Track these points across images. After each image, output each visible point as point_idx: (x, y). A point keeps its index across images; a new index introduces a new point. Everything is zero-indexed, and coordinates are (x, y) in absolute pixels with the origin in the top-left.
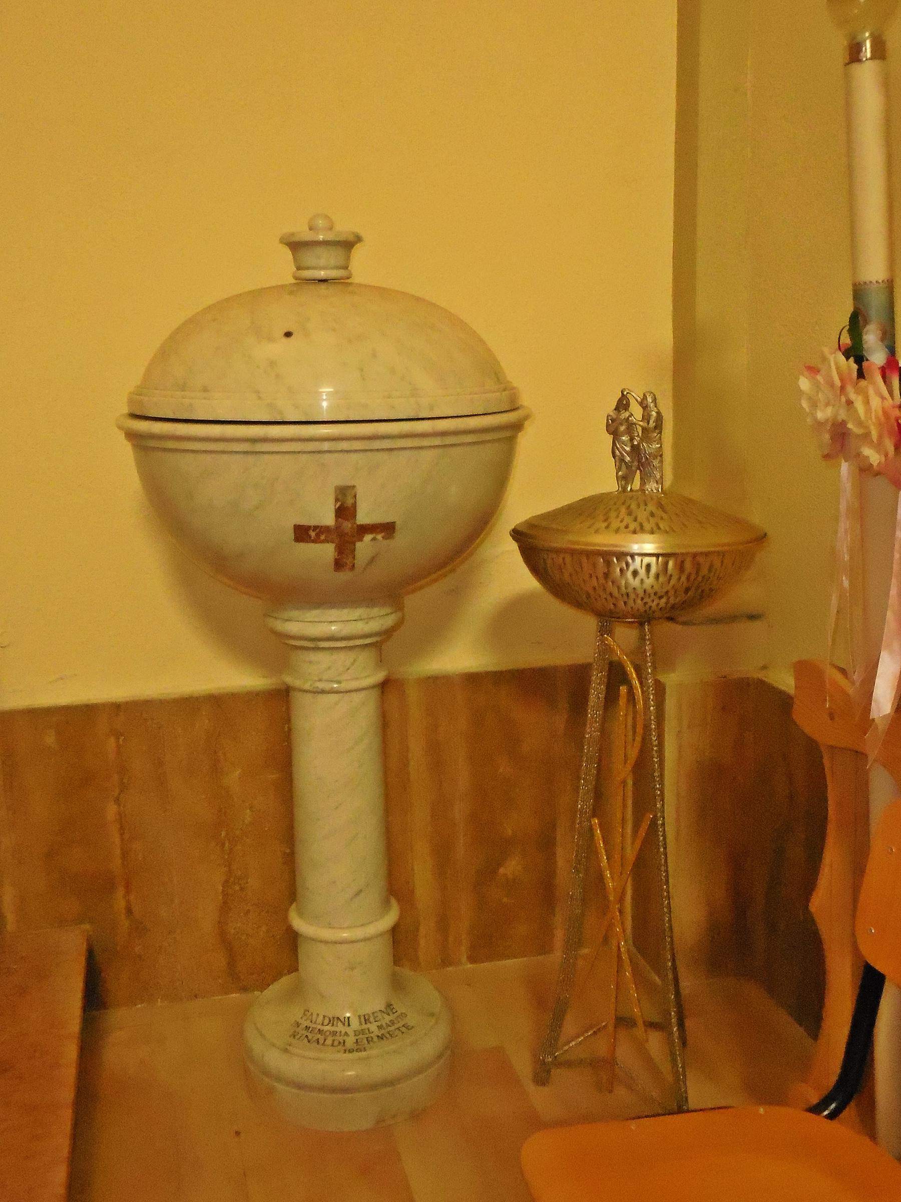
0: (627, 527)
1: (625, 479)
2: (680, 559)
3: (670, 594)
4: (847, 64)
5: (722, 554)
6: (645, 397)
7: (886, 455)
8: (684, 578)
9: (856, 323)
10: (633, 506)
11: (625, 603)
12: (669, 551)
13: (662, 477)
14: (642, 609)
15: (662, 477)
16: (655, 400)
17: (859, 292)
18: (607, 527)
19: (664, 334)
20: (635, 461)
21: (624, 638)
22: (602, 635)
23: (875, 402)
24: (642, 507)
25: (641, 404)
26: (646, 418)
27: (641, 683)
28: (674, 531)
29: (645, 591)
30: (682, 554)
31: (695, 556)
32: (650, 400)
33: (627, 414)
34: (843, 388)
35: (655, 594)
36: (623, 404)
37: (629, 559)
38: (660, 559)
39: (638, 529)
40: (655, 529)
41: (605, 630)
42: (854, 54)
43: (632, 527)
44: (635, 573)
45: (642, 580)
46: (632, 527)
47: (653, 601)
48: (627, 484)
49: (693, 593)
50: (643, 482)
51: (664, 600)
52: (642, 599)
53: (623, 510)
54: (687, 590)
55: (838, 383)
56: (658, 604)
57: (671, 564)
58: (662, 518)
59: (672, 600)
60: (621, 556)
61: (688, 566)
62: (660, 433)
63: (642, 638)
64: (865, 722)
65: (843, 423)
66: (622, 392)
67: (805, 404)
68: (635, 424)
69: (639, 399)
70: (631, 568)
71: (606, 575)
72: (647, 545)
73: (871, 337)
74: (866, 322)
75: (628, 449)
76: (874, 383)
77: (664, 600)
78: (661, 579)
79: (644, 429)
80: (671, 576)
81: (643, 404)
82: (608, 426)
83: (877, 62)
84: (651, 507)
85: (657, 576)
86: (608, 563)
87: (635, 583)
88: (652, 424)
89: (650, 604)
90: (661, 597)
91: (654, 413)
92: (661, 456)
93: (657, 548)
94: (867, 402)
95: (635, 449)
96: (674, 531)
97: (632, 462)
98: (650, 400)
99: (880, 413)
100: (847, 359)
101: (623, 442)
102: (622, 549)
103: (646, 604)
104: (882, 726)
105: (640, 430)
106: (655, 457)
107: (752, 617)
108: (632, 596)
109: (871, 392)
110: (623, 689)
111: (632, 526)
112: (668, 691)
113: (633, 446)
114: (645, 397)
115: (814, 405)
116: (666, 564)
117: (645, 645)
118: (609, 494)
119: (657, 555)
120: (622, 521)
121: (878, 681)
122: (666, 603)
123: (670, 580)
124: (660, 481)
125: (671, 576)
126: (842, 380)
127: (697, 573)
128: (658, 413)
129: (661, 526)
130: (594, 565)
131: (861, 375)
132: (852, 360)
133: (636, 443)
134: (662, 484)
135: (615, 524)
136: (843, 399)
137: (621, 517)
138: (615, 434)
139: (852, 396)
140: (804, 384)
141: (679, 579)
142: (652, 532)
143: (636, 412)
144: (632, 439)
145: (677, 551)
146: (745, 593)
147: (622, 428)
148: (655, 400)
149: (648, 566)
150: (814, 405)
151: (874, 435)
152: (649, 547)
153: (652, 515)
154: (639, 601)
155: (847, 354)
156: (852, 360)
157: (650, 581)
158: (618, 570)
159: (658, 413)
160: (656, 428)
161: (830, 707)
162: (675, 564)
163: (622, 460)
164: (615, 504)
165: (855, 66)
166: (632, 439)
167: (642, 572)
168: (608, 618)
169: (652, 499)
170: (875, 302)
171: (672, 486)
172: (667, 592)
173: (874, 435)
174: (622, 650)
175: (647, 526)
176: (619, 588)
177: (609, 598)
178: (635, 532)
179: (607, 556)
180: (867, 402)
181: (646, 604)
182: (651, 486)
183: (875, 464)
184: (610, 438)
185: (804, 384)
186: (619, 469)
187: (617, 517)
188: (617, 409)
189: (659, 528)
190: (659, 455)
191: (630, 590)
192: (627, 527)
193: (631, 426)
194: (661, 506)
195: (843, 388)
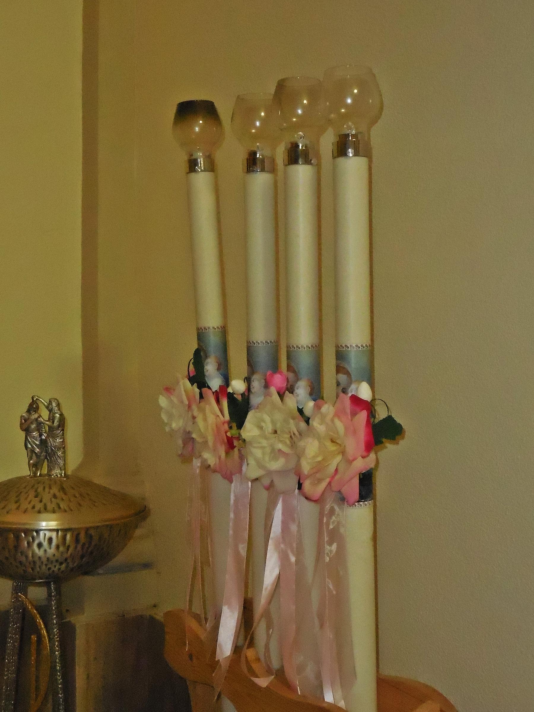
0: (33, 507)
1: (36, 466)
2: (75, 533)
3: (69, 561)
4: (188, 173)
5: (111, 526)
6: (50, 403)
7: (220, 458)
8: (79, 547)
9: (199, 358)
10: (40, 489)
11: (33, 569)
12: (66, 526)
13: (64, 465)
14: (47, 572)
15: (64, 465)
16: (58, 405)
17: (201, 335)
18: (18, 508)
19: (75, 345)
20: (44, 454)
21: (37, 593)
22: (17, 593)
23: (211, 419)
24: (47, 490)
25: (47, 407)
26: (52, 419)
27: (48, 632)
28: (71, 510)
29: (48, 559)
30: (78, 529)
31: (87, 529)
32: (54, 404)
33: (36, 416)
34: (189, 406)
35: (57, 561)
36: (33, 407)
37: (35, 534)
38: (60, 533)
39: (42, 509)
40: (56, 509)
41: (20, 589)
42: (192, 165)
43: (37, 508)
44: (40, 545)
45: (45, 551)
46: (37, 508)
47: (55, 566)
48: (37, 469)
49: (92, 553)
50: (50, 470)
51: (64, 566)
52: (46, 565)
53: (32, 494)
54: (82, 557)
55: (187, 402)
56: (59, 569)
57: (68, 537)
58: (63, 499)
59: (71, 565)
60: (28, 532)
61: (82, 536)
62: (63, 430)
63: (50, 595)
64: (214, 664)
65: (189, 433)
66: (33, 398)
67: (164, 417)
68: (42, 423)
69: (46, 404)
70: (36, 542)
71: (16, 547)
72: (48, 524)
73: (210, 367)
74: (207, 357)
75: (38, 443)
76: (210, 404)
77: (63, 566)
78: (61, 549)
79: (50, 427)
80: (69, 546)
81: (49, 408)
82: (21, 424)
83: (207, 173)
84: (55, 490)
85: (58, 547)
86: (18, 538)
87: (40, 553)
88: (56, 423)
89: (53, 568)
90: (61, 564)
91: (58, 415)
92: (64, 448)
93: (57, 525)
94: (205, 419)
95: (44, 443)
96: (71, 510)
97: (41, 453)
98: (54, 404)
99: (214, 426)
100: (192, 385)
101: (34, 437)
102: (27, 527)
103: (49, 569)
104: (224, 666)
105: (47, 428)
106: (59, 449)
107: (147, 566)
108: (38, 564)
109: (207, 411)
110: (34, 638)
111: (39, 506)
112: (78, 631)
113: (41, 440)
114: (50, 403)
115: (171, 416)
116: (64, 538)
117: (51, 600)
118: (20, 479)
119: (57, 531)
120: (30, 503)
121: (221, 630)
122: (67, 567)
123: (68, 549)
124: (64, 468)
125: (69, 546)
126: (188, 399)
127: (90, 543)
128: (61, 415)
129: (61, 506)
130: (7, 539)
131: (201, 396)
132: (195, 384)
133: (43, 437)
134: (65, 469)
135: (25, 505)
136: (190, 414)
137: (29, 499)
138: (27, 431)
139: (196, 413)
140: (163, 401)
141: (76, 547)
142: (54, 512)
143: (45, 414)
144: (41, 435)
145: (73, 526)
146: (137, 548)
147: (33, 426)
148: (58, 405)
149: (50, 540)
150: (171, 416)
151: (210, 443)
152: (53, 524)
153: (55, 496)
154: (44, 567)
155: (192, 380)
156: (195, 384)
157: (52, 551)
158: (26, 543)
159: (61, 415)
160: (59, 426)
161: (189, 650)
162: (72, 536)
163: (33, 451)
164: (25, 488)
165: (193, 175)
166: (41, 435)
167: (45, 544)
168: (23, 579)
169: (55, 483)
170: (213, 340)
171: (81, 466)
172: (66, 560)
173: (210, 443)
174: (32, 605)
175: (50, 506)
176: (27, 557)
177: (19, 565)
178: (39, 512)
179: (17, 532)
180: (205, 419)
181: (49, 569)
182: (56, 472)
183: (212, 465)
184: (23, 434)
185: (163, 401)
186: (31, 458)
187: (26, 499)
188: (29, 411)
189: (60, 508)
190: (63, 447)
191: (36, 559)
192: (33, 507)
193: (40, 425)
194: (62, 489)
195: (189, 406)
